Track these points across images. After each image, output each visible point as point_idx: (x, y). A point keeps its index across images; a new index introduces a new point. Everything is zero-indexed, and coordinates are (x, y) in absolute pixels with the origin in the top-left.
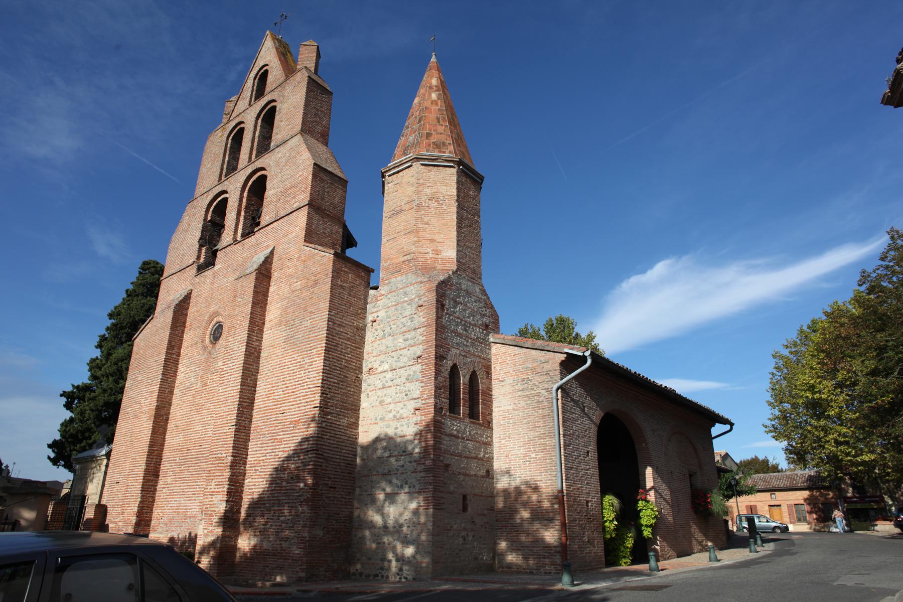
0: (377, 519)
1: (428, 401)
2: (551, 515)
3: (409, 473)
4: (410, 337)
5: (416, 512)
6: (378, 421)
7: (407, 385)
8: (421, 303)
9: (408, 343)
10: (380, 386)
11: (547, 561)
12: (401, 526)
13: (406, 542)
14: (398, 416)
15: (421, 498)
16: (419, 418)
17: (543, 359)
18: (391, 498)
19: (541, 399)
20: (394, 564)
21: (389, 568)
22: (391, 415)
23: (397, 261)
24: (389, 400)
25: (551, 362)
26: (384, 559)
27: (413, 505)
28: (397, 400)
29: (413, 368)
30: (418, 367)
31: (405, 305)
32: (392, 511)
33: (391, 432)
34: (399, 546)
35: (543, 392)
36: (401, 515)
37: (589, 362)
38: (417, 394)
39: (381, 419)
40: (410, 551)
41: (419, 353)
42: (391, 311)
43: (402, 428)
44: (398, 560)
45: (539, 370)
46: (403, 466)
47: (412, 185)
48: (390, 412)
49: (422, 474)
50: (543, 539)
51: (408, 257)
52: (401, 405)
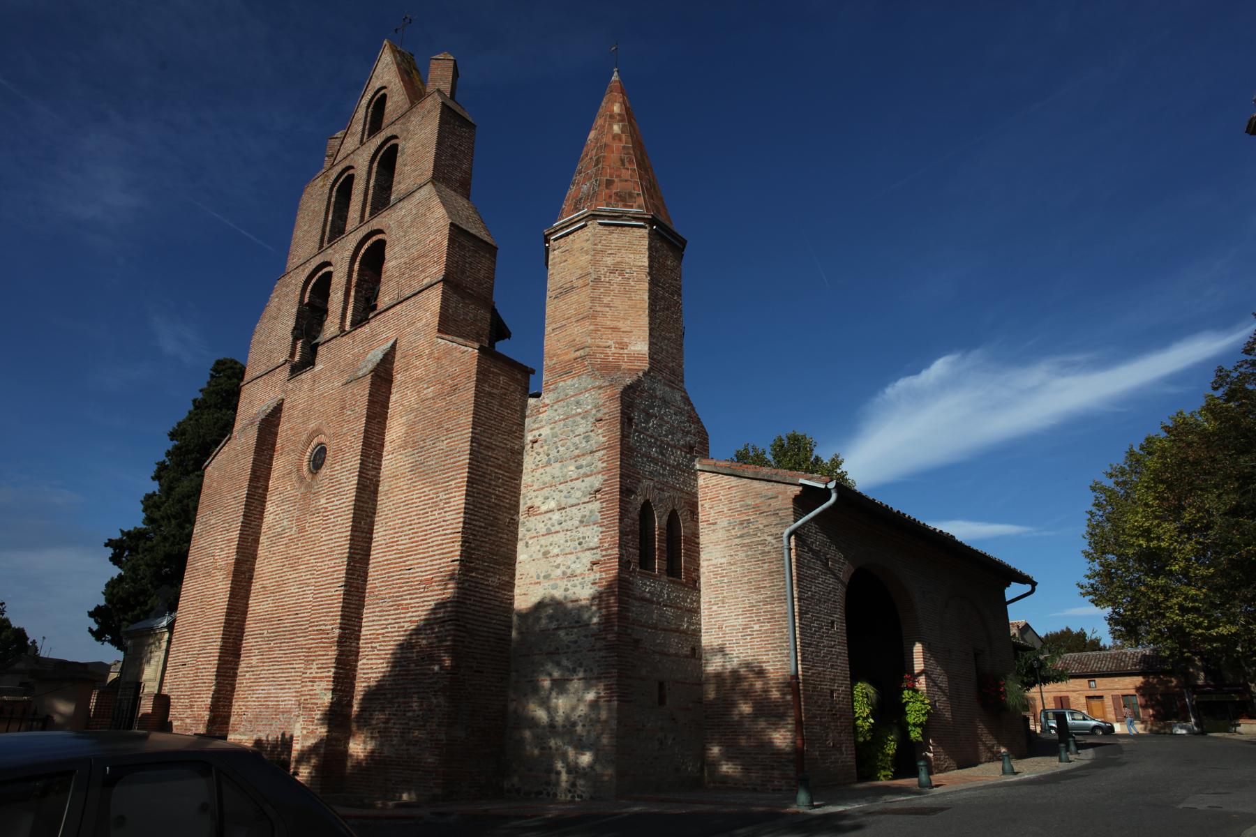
4: (584, 463)
7: (581, 529)
9: (582, 471)
14: (569, 572)
16: (598, 576)
17: (770, 494)
19: (767, 549)
24: (556, 551)
28: (568, 551)
29: (590, 506)
30: (596, 506)
31: (578, 418)
35: (769, 538)
38: (595, 541)
41: (597, 486)
48: (558, 567)
52: (573, 557)
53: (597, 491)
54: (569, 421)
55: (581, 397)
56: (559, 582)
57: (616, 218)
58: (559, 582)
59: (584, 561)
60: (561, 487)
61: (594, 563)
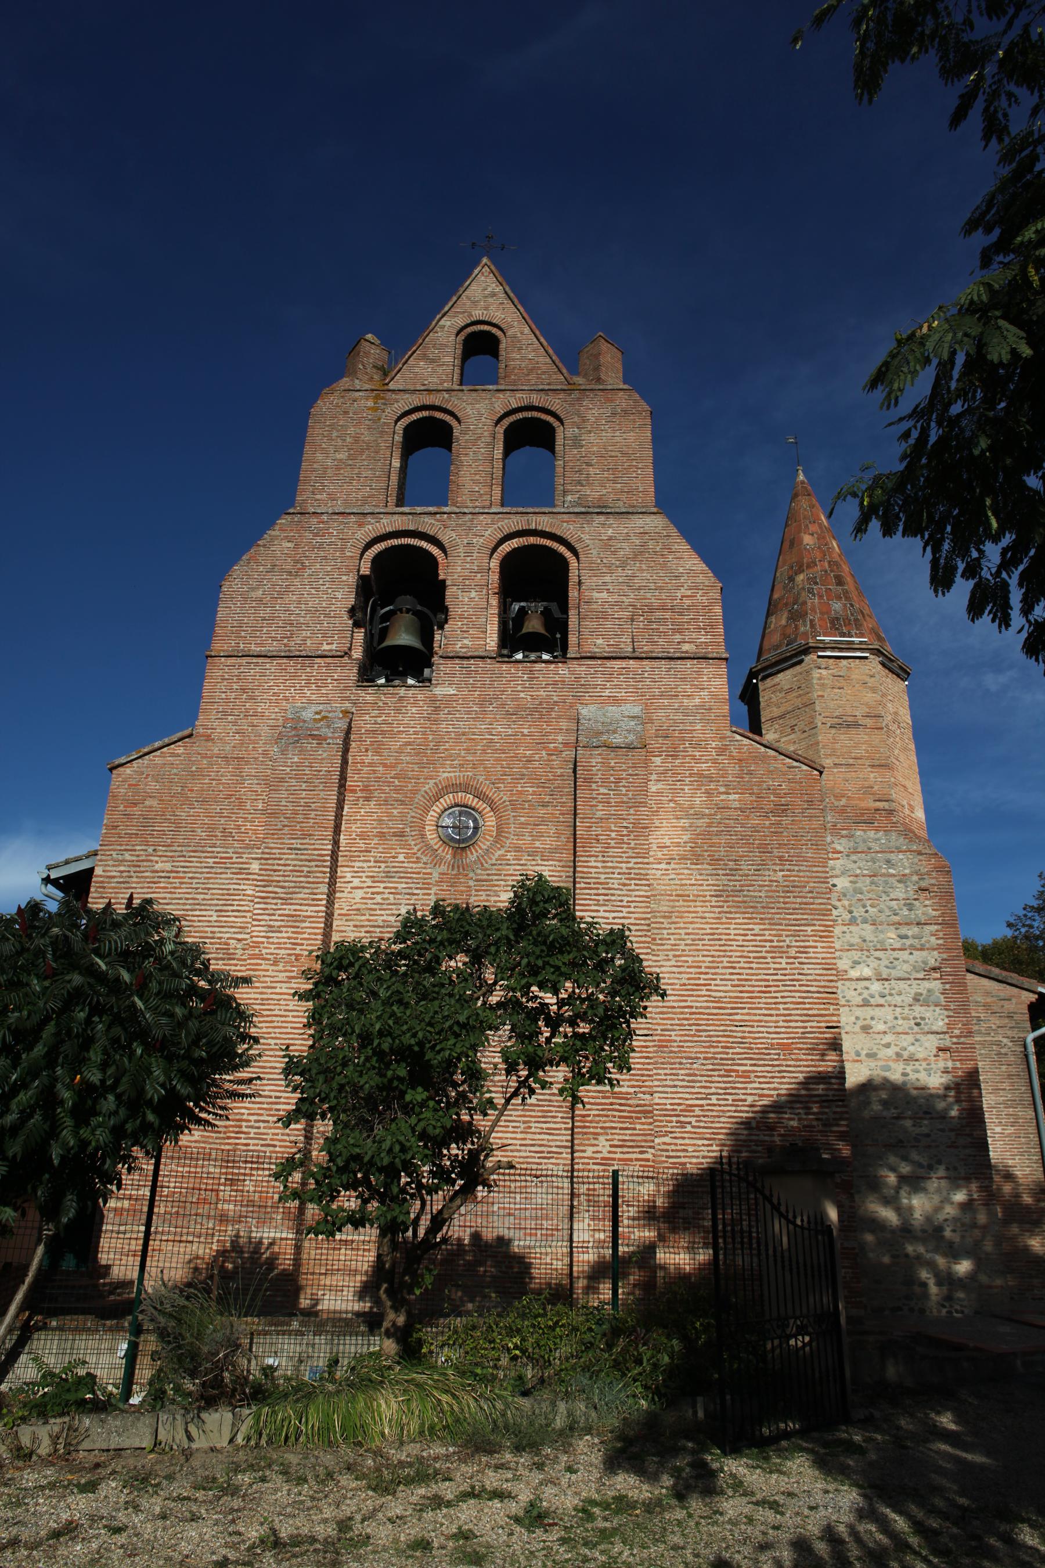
0: (888, 1215)
1: (962, 1040)
2: (1035, 1216)
4: (910, 933)
5: (966, 1206)
6: (863, 1057)
7: (917, 1008)
8: (923, 884)
9: (908, 942)
10: (858, 1000)
12: (939, 1229)
13: (954, 1253)
14: (906, 1054)
15: (974, 1186)
17: (1002, 995)
18: (914, 1182)
19: (1003, 1051)
20: (933, 1289)
21: (926, 1295)
22: (890, 1052)
23: (863, 804)
24: (881, 1027)
25: (1014, 1001)
26: (912, 1281)
27: (960, 1197)
28: (900, 1029)
29: (926, 984)
31: (892, 880)
32: (919, 1204)
33: (895, 1076)
34: (941, 1261)
35: (1005, 1040)
36: (938, 1209)
38: (940, 1025)
39: (868, 1055)
40: (964, 1267)
41: (932, 963)
42: (864, 883)
43: (917, 1075)
44: (939, 1284)
45: (995, 1009)
46: (928, 1135)
48: (888, 1046)
50: (1027, 1249)
52: (910, 1038)
53: (934, 969)
56: (891, 1063)
59: (927, 1044)
60: (878, 954)
61: (940, 1049)
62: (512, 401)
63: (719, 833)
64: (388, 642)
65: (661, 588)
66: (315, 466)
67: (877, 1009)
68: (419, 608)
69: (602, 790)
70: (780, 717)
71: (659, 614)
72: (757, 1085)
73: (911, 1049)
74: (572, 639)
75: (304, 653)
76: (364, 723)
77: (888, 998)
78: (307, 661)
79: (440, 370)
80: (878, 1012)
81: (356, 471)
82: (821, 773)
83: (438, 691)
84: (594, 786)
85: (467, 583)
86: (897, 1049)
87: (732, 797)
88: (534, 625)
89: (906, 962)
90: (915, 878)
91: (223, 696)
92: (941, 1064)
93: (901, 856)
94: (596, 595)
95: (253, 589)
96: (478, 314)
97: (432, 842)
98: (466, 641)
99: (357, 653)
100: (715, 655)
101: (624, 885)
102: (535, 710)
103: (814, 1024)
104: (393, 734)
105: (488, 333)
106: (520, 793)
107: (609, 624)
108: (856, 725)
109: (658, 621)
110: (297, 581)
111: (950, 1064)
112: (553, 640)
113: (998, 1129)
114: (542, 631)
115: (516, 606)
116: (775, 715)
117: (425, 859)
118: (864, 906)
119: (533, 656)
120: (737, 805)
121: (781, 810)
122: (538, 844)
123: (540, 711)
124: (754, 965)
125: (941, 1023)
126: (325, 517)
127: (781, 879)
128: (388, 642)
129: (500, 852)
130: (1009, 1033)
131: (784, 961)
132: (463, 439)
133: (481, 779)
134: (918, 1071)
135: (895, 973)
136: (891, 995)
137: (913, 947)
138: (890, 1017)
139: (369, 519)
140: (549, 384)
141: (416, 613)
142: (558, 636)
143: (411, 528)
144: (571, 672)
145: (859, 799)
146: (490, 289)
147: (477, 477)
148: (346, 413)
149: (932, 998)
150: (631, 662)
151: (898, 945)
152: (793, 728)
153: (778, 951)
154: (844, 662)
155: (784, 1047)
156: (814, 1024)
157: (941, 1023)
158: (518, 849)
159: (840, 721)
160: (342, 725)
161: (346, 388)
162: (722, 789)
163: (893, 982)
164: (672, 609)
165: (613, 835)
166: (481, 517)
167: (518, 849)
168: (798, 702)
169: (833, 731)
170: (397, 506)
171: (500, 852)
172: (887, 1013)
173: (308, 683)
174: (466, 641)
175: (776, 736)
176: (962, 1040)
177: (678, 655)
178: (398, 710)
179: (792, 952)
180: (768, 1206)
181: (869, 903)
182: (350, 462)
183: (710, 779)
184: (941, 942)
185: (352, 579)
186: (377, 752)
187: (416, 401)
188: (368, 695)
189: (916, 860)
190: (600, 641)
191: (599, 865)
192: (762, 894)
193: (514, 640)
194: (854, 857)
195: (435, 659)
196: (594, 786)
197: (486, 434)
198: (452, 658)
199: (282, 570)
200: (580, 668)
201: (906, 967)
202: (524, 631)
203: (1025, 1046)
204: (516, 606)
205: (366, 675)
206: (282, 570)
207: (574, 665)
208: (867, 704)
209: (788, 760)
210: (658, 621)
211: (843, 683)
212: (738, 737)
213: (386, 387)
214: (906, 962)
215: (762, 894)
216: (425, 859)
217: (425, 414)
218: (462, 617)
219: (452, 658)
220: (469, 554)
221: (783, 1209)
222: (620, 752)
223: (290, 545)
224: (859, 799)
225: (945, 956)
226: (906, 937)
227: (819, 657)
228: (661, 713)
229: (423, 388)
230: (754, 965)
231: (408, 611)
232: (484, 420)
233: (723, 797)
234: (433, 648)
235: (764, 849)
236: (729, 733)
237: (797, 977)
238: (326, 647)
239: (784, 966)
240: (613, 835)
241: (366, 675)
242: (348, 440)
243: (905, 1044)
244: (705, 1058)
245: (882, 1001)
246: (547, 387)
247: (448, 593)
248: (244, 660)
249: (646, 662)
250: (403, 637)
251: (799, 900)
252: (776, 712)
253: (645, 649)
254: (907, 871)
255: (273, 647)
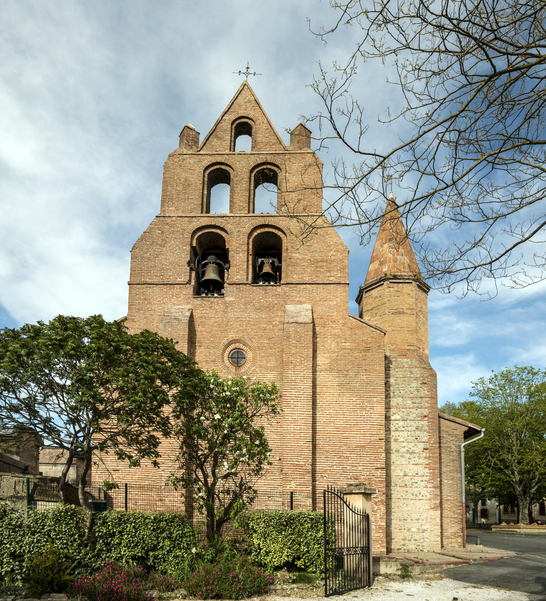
1: (434, 445)
3: (422, 488)
4: (417, 401)
7: (417, 432)
8: (425, 381)
9: (416, 405)
11: (453, 540)
14: (411, 451)
16: (428, 455)
17: (454, 428)
19: (451, 450)
22: (404, 450)
23: (403, 347)
24: (402, 439)
28: (409, 441)
29: (421, 422)
30: (425, 423)
31: (412, 379)
35: (453, 446)
37: (482, 435)
38: (426, 439)
41: (425, 414)
46: (417, 483)
47: (412, 297)
48: (404, 447)
49: (432, 489)
51: (412, 348)
52: (413, 444)
53: (425, 416)
54: (406, 379)
55: (413, 370)
56: (405, 454)
57: (378, 283)
58: (405, 454)
59: (419, 447)
60: (403, 410)
61: (425, 449)
62: (258, 159)
63: (341, 360)
64: (206, 278)
65: (322, 251)
66: (168, 193)
67: (401, 432)
68: (218, 261)
69: (294, 342)
70: (371, 310)
71: (320, 264)
72: (351, 462)
73: (413, 448)
74: (283, 275)
75: (169, 283)
76: (196, 315)
77: (406, 428)
78: (172, 286)
79: (224, 143)
80: (401, 434)
81: (187, 196)
82: (385, 334)
83: (227, 299)
84: (291, 340)
85: (238, 249)
86: (407, 448)
87: (347, 344)
88: (267, 269)
89: (415, 413)
90: (421, 379)
91: (137, 302)
92: (424, 455)
93: (416, 369)
94: (294, 255)
95: (146, 253)
96: (242, 113)
97: (227, 364)
98: (238, 277)
99: (193, 283)
100: (343, 282)
101: (302, 381)
102: (267, 307)
103: (374, 438)
104: (210, 318)
105: (247, 123)
106: (261, 343)
107: (299, 268)
108: (403, 313)
109: (321, 267)
110: (164, 249)
111: (428, 455)
112: (274, 277)
113: (446, 481)
114: (271, 271)
115: (260, 260)
116: (369, 309)
117: (224, 371)
118: (399, 390)
119: (267, 284)
120: (349, 347)
121: (367, 349)
122: (268, 364)
123: (269, 308)
124: (352, 414)
125: (426, 438)
126: (174, 218)
127: (365, 379)
128: (206, 278)
129: (254, 368)
130: (455, 443)
131: (364, 412)
132: (235, 179)
133: (246, 337)
134: (415, 458)
135: (410, 418)
136: (407, 427)
137: (418, 407)
138: (406, 435)
139: (194, 219)
140: (275, 151)
141: (217, 264)
142: (278, 274)
143: (213, 224)
144: (283, 290)
145: (401, 345)
146: (247, 98)
147: (242, 199)
148: (180, 166)
149: (423, 428)
150: (308, 285)
151: (411, 406)
152: (376, 314)
153: (363, 408)
154: (401, 285)
155: (362, 447)
156: (374, 438)
157: (426, 438)
158: (261, 367)
159: (396, 311)
160: (188, 314)
161: (180, 153)
162: (343, 341)
163: (408, 421)
164: (326, 261)
165: (298, 360)
166: (244, 218)
167: (261, 367)
168: (379, 303)
169: (393, 315)
170: (206, 213)
171: (254, 368)
172: (405, 434)
173: (173, 295)
174: (238, 277)
175: (369, 318)
176: (434, 445)
177: (327, 282)
178: (211, 308)
179: (368, 409)
180: (345, 506)
181: (401, 389)
182: (184, 191)
183: (339, 336)
184: (429, 405)
185: (188, 248)
186: (203, 326)
187: (213, 160)
188: (198, 301)
189: (422, 371)
190: (295, 276)
191: (292, 373)
192: (357, 385)
193: (259, 277)
194: (397, 370)
195: (225, 285)
196: (291, 340)
197: (246, 177)
198: (233, 284)
199: (157, 244)
200: (286, 288)
201: (414, 415)
202: (263, 272)
203: (460, 448)
204: (260, 260)
205: (197, 293)
206: (157, 244)
207: (283, 286)
208: (409, 304)
209: (371, 328)
210: (321, 267)
211: (399, 294)
212: (351, 318)
213: (199, 153)
214: (415, 413)
215: (357, 385)
216: (224, 371)
217: (218, 167)
218: (236, 266)
219: (233, 284)
220: (238, 236)
221: (351, 507)
222: (302, 325)
223: (159, 232)
224: (401, 345)
225: (430, 411)
226: (415, 403)
227: (390, 282)
228: (320, 308)
229: (216, 153)
230: (352, 414)
231: (213, 263)
232: (245, 169)
233: (343, 344)
234: (224, 280)
235: (359, 366)
236: (348, 317)
237: (369, 419)
238: (179, 280)
239: (364, 414)
240: (298, 360)
241: (197, 293)
242: (182, 180)
243: (411, 446)
244: (332, 451)
245: (403, 429)
246: (274, 152)
247: (230, 254)
248: (145, 286)
249: (314, 286)
250: (211, 274)
251: (372, 387)
252: (370, 307)
253: (314, 279)
254: (418, 376)
255: (156, 280)
